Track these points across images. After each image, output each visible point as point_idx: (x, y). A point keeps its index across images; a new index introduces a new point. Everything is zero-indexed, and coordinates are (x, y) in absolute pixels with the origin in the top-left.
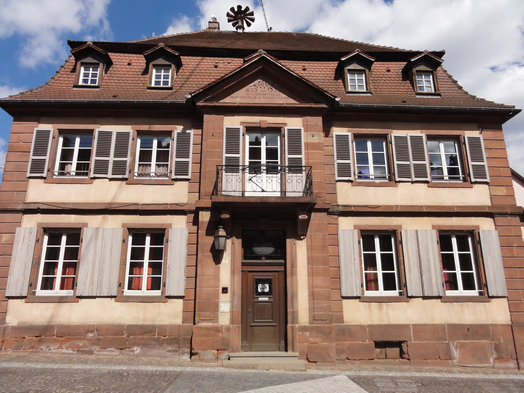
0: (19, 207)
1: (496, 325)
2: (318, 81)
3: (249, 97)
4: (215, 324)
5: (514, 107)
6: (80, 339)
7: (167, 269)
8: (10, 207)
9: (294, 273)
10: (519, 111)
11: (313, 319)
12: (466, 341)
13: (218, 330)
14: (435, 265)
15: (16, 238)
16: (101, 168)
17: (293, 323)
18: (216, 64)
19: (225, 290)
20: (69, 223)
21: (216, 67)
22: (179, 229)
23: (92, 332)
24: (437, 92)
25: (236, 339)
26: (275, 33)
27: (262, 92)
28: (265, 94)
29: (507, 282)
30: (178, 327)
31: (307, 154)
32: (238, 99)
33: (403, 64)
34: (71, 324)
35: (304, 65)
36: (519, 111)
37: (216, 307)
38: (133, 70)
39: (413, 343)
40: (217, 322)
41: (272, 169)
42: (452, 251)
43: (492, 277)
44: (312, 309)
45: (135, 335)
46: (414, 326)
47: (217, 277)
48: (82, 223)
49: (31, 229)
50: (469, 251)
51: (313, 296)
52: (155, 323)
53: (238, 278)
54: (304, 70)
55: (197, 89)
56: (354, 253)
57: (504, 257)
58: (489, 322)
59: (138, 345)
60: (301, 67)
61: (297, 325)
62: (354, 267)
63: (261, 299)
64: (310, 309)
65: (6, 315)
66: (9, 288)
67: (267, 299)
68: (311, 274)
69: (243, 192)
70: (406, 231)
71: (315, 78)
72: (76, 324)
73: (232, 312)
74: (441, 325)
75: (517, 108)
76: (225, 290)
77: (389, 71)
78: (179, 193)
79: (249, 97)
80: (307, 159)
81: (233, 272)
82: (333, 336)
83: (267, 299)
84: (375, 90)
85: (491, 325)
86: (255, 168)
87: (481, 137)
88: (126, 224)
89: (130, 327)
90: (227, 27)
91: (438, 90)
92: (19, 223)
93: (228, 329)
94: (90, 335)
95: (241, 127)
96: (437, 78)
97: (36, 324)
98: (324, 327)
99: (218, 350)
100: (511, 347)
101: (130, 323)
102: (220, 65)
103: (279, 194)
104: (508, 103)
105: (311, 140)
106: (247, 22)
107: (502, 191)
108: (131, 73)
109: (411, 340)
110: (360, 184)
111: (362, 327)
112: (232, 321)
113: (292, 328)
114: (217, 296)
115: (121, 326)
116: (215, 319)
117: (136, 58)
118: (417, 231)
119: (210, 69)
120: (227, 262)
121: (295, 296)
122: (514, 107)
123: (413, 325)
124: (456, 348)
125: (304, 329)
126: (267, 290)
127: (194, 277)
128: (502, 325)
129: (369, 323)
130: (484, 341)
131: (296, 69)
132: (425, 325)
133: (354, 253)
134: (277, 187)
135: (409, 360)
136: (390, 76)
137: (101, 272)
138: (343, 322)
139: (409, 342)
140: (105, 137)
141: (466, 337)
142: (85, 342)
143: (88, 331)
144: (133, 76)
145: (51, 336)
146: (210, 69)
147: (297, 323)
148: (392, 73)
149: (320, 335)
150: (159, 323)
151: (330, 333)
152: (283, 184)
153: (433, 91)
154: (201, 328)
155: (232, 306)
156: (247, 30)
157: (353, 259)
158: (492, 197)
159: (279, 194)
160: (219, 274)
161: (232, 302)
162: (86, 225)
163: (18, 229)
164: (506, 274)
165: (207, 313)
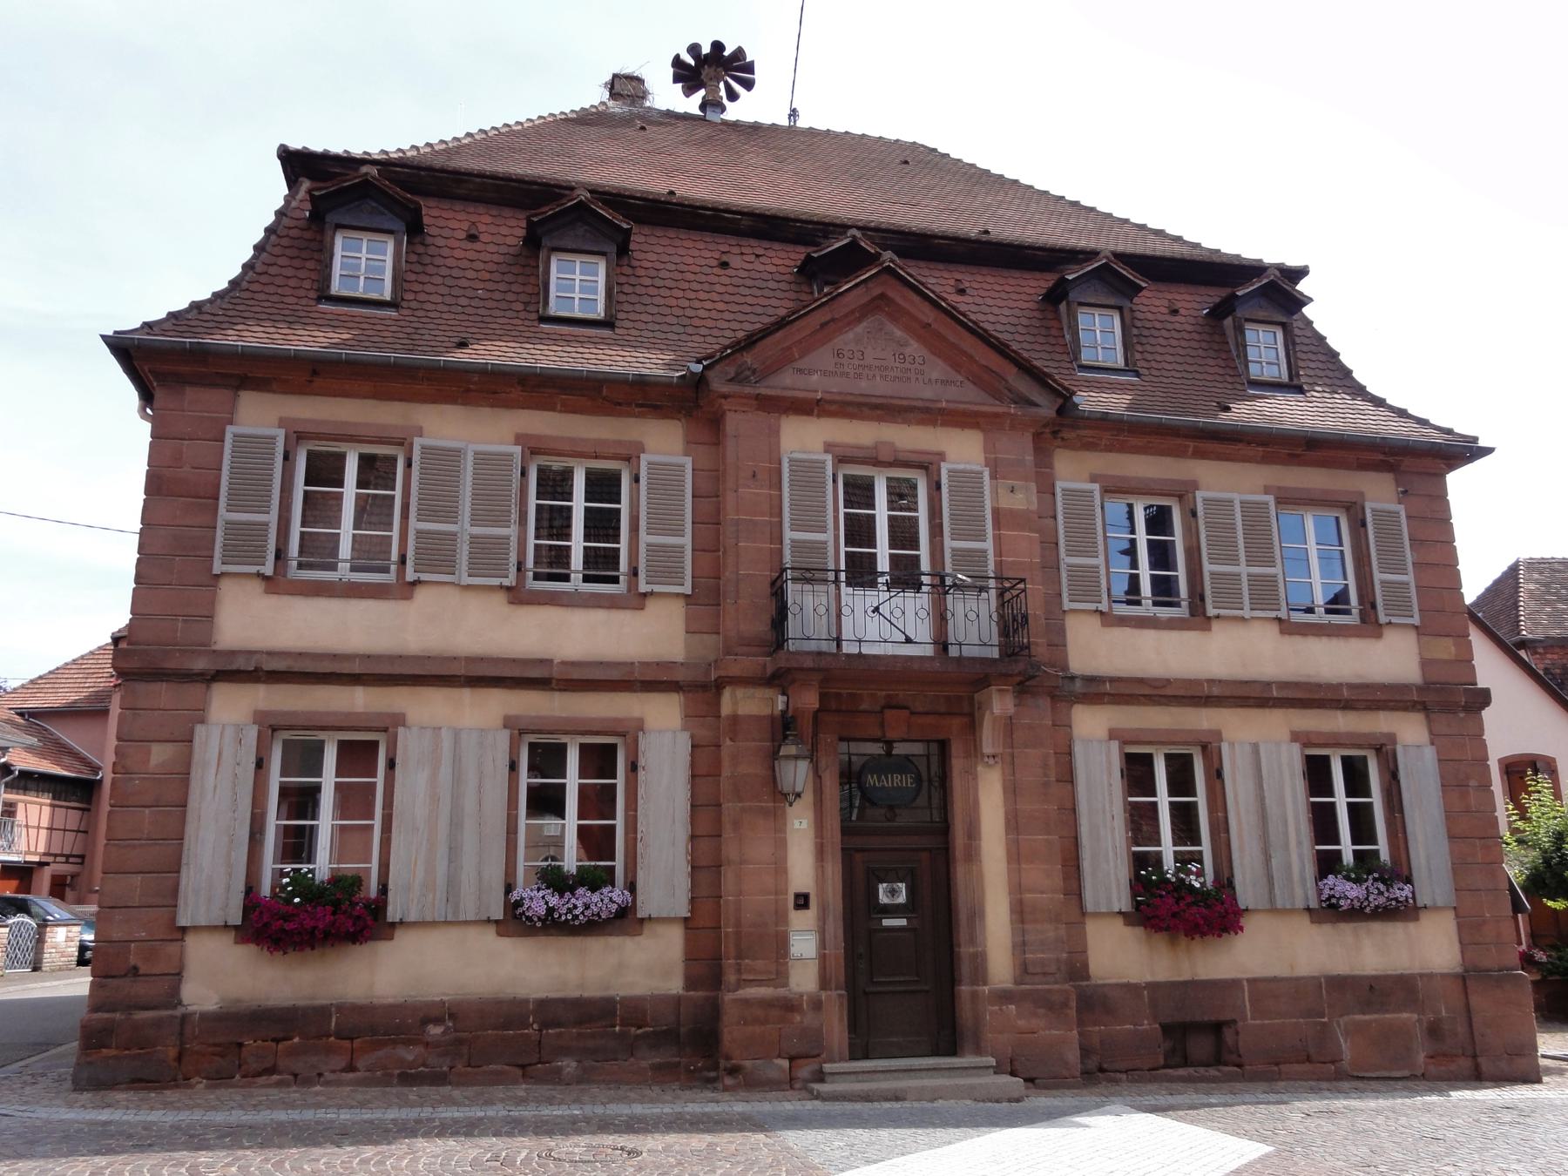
0: (200, 664)
1: (1431, 976)
2: (999, 327)
3: (842, 374)
4: (781, 992)
5: (1475, 439)
6: (408, 1043)
7: (639, 845)
8: (171, 664)
9: (973, 855)
10: (1489, 451)
11: (1024, 970)
12: (1367, 1017)
13: (789, 1006)
14: (1298, 831)
15: (196, 757)
16: (438, 555)
17: (974, 982)
18: (725, 258)
19: (802, 901)
20: (349, 714)
21: (724, 265)
22: (664, 734)
23: (438, 1021)
24: (1295, 382)
25: (835, 1027)
26: (811, 132)
27: (877, 363)
28: (886, 368)
29: (1455, 871)
30: (678, 1000)
31: (998, 539)
32: (815, 377)
33: (1215, 295)
34: (375, 1001)
35: (959, 276)
36: (1489, 451)
37: (781, 945)
38: (483, 256)
39: (1251, 1022)
40: (786, 985)
41: (905, 577)
42: (1332, 795)
43: (1423, 861)
44: (1020, 946)
45: (559, 1025)
46: (1253, 982)
47: (780, 868)
48: (389, 715)
49: (239, 729)
50: (1369, 795)
51: (1020, 912)
52: (611, 993)
53: (834, 870)
54: (962, 292)
55: (717, 347)
56: (1111, 802)
57: (1450, 816)
58: (1417, 969)
59: (565, 1051)
60: (952, 282)
61: (986, 989)
62: (457, 760)
63: (886, 922)
64: (1014, 946)
65: (180, 981)
66: (186, 904)
67: (903, 922)
68: (1015, 856)
69: (839, 640)
70: (1232, 744)
71: (992, 318)
72: (391, 1000)
73: (823, 958)
74: (1313, 978)
75: (1481, 443)
76: (802, 901)
77: (1175, 312)
78: (653, 632)
79: (842, 374)
80: (999, 552)
81: (820, 853)
82: (1073, 1013)
83: (903, 922)
84: (1145, 364)
85: (1421, 975)
86: (861, 572)
87: (1401, 509)
88: (517, 718)
89: (543, 1004)
90: (667, 96)
91: (1298, 375)
92: (200, 715)
93: (817, 1005)
94: (435, 1031)
95: (829, 458)
96: (1294, 344)
97: (271, 1003)
98: (1049, 991)
99: (792, 1059)
100: (1461, 1029)
101: (542, 995)
102: (735, 261)
103: (928, 651)
104: (1463, 426)
105: (1007, 502)
106: (729, 88)
107: (1444, 649)
108: (481, 266)
109: (1245, 1019)
110: (1123, 621)
111: (1132, 989)
112: (824, 983)
113: (974, 995)
114: (781, 918)
115: (519, 1003)
116: (780, 976)
117: (488, 219)
118: (1255, 748)
119: (709, 270)
120: (805, 825)
121: (977, 914)
122: (1475, 439)
123: (1248, 980)
124: (1347, 1034)
125: (1005, 997)
126: (902, 899)
127: (707, 868)
128: (1444, 976)
129: (1149, 978)
130: (1405, 1015)
131: (974, 308)
132: (1275, 980)
133: (1111, 802)
134: (922, 631)
135: (1240, 1066)
136: (1178, 326)
137: (454, 852)
138: (1088, 978)
139: (1240, 1024)
140: (444, 461)
141: (1366, 1006)
142: (419, 1049)
143: (426, 1021)
144: (487, 276)
145: (319, 1037)
146: (709, 270)
147: (985, 984)
148: (1182, 319)
149: (1041, 1011)
150: (622, 993)
151: (1065, 1005)
152: (941, 618)
153: (1285, 378)
154: (746, 1002)
155: (822, 944)
156: (734, 112)
157: (1108, 816)
158: (1425, 664)
159: (928, 651)
160: (784, 859)
161: (822, 932)
162: (399, 720)
163: (200, 730)
164: (1452, 852)
165: (760, 964)
